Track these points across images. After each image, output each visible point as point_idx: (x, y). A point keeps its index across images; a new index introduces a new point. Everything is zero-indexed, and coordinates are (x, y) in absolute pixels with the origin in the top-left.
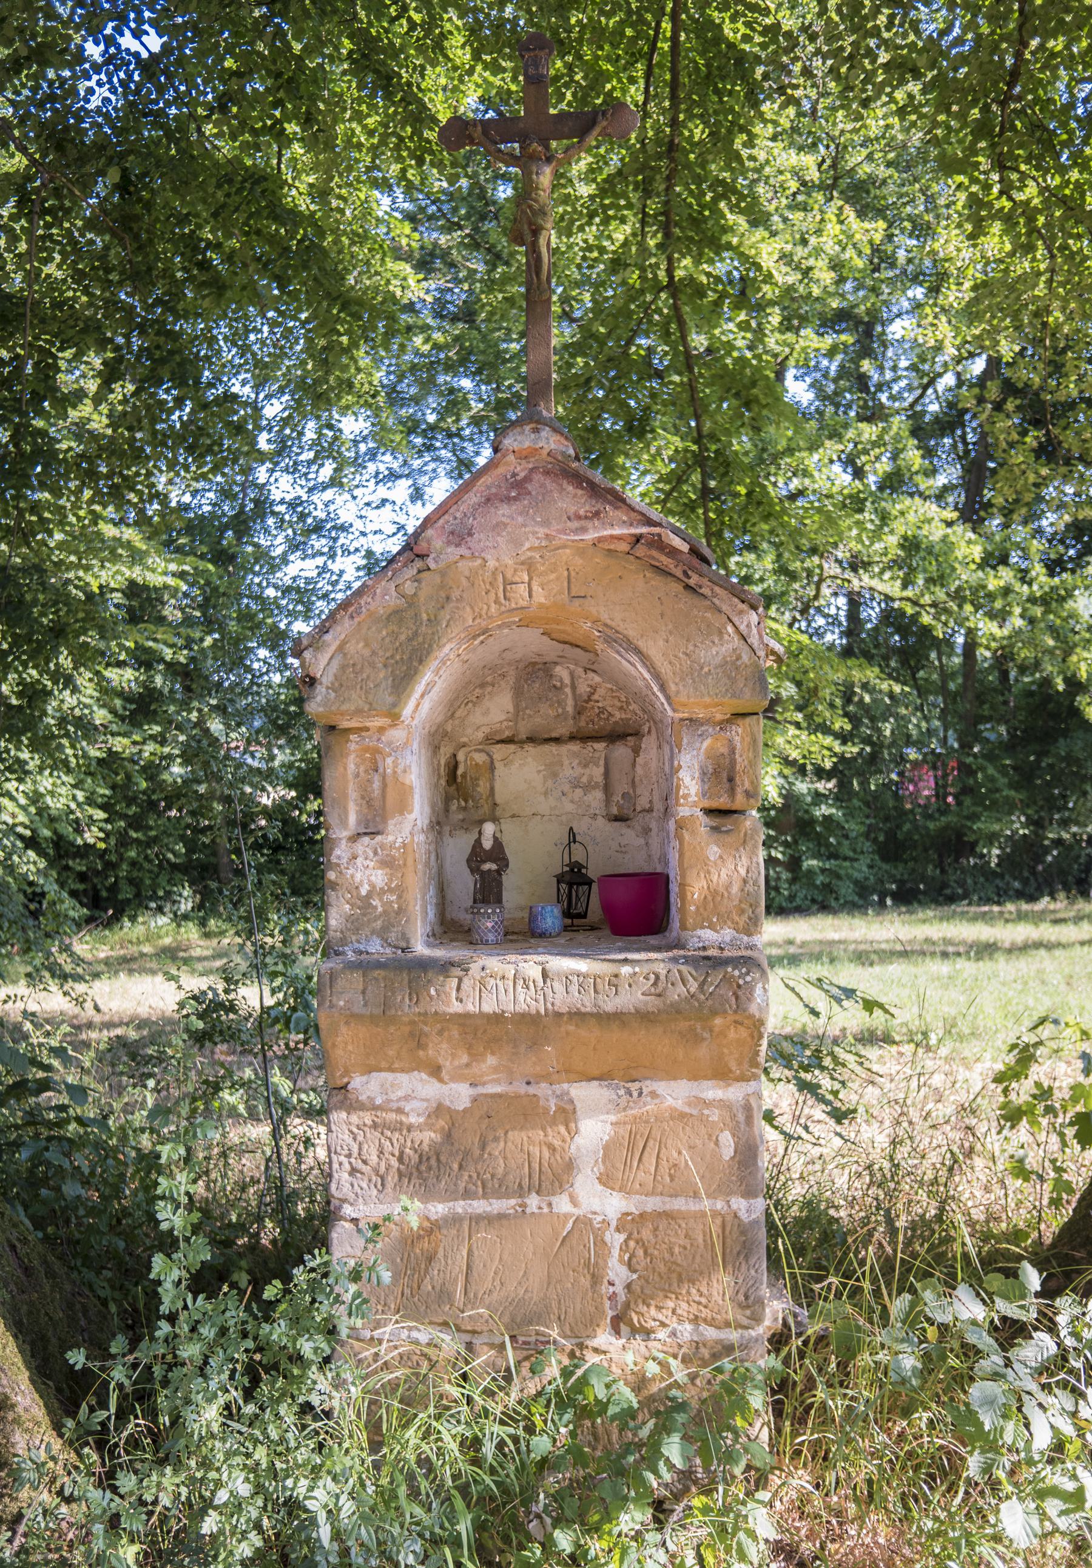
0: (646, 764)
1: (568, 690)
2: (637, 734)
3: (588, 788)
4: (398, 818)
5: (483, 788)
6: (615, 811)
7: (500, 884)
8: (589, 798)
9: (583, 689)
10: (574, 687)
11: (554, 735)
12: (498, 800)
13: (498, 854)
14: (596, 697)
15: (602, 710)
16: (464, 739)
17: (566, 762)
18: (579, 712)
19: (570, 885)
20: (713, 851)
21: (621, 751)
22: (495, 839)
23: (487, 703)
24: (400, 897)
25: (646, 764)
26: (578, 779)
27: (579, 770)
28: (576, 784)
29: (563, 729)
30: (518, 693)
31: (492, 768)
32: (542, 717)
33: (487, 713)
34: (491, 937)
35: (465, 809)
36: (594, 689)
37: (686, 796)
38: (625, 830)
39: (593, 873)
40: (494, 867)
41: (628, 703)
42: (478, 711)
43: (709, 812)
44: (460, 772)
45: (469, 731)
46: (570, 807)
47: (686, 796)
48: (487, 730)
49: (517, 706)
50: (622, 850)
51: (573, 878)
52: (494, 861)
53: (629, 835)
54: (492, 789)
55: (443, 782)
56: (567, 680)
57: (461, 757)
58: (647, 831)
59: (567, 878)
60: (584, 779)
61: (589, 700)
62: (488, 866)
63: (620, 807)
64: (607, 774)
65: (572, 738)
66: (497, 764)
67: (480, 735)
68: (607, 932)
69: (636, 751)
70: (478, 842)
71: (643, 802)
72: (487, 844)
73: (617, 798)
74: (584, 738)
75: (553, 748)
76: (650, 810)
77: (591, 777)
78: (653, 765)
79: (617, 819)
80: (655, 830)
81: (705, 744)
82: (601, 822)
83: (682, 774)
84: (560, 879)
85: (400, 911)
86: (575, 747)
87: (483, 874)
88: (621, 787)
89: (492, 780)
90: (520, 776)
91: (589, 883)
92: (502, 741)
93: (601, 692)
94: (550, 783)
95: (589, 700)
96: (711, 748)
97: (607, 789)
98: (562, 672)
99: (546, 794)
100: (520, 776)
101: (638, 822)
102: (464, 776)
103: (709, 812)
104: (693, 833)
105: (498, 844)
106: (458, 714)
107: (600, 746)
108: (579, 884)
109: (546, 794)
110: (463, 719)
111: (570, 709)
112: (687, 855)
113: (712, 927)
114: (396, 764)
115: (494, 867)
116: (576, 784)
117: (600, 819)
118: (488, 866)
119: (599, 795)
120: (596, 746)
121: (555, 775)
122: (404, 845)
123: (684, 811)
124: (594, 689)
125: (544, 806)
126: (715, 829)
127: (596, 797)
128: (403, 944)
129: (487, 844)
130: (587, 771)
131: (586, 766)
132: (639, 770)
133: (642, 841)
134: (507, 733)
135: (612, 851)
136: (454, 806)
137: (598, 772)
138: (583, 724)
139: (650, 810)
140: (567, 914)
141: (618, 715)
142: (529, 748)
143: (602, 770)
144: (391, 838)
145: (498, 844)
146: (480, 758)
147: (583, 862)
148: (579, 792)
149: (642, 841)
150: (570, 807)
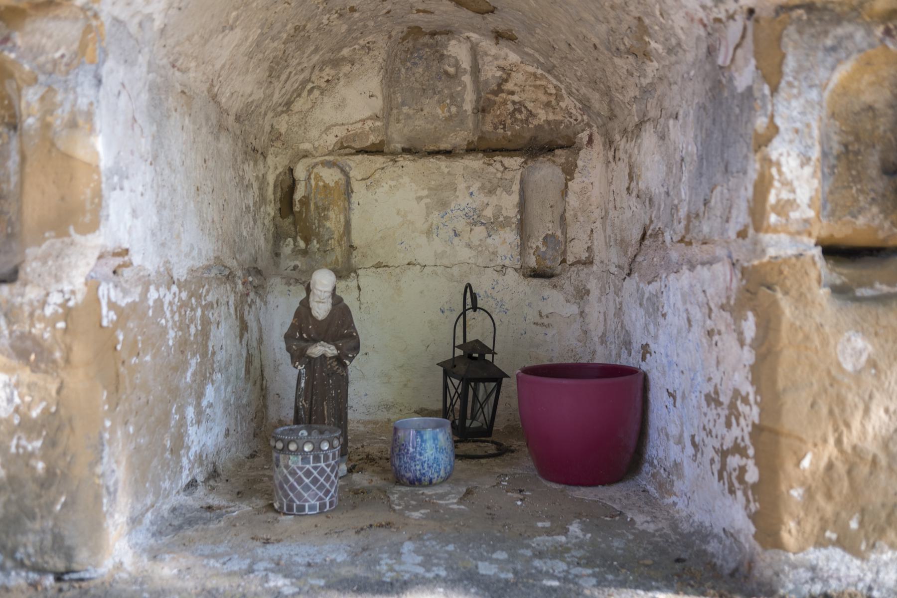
0: (584, 191)
1: (467, 79)
2: (570, 145)
3: (494, 225)
4: (51, 243)
5: (333, 222)
6: (532, 262)
7: (343, 383)
8: (495, 241)
9: (491, 72)
10: (476, 70)
11: (443, 146)
12: (356, 240)
13: (340, 327)
14: (509, 86)
15: (519, 107)
16: (306, 146)
17: (461, 186)
18: (482, 109)
19: (466, 381)
20: (853, 348)
21: (546, 172)
22: (337, 300)
23: (342, 90)
24: (51, 443)
25: (584, 191)
26: (478, 212)
27: (481, 198)
28: (475, 219)
29: (459, 138)
30: (391, 79)
31: (348, 192)
32: (426, 118)
33: (341, 105)
34: (311, 501)
35: (305, 253)
36: (507, 73)
37: (783, 208)
38: (548, 292)
39: (500, 361)
40: (331, 350)
41: (559, 97)
42: (328, 102)
43: (834, 252)
44: (299, 195)
45: (314, 133)
46: (465, 254)
47: (783, 208)
48: (341, 132)
49: (388, 98)
50: (543, 321)
51: (471, 367)
52: (331, 339)
53: (555, 300)
54: (348, 224)
55: (271, 210)
56: (466, 64)
57: (300, 172)
58: (582, 294)
59: (461, 368)
60: (489, 213)
61: (499, 90)
62: (318, 350)
63: (540, 257)
64: (522, 206)
65: (471, 150)
66: (356, 186)
67: (331, 140)
68: (525, 465)
69: (569, 171)
70: (305, 305)
71: (577, 250)
72: (321, 309)
73: (537, 243)
74: (486, 148)
75: (443, 164)
76: (589, 262)
77: (499, 208)
78: (596, 193)
79: (537, 274)
80: (595, 292)
81: (838, 76)
82: (512, 277)
83: (778, 149)
84: (449, 369)
85: (49, 480)
86: (475, 163)
87: (311, 363)
88: (543, 225)
89: (347, 210)
90: (391, 206)
91: (498, 377)
92: (360, 152)
93: (518, 78)
94: (435, 217)
95: (499, 90)
96: (843, 90)
97: (523, 228)
98: (458, 51)
99: (429, 233)
100: (391, 206)
101: (570, 279)
102: (305, 201)
103: (834, 252)
104: (801, 299)
105: (339, 307)
106: (298, 105)
107: (514, 162)
108: (478, 380)
109: (429, 233)
110: (304, 115)
111: (468, 107)
112: (788, 355)
113: (847, 543)
114: (48, 104)
115: (331, 350)
116: (475, 219)
117: (511, 272)
118: (318, 350)
119: (510, 236)
120: (507, 161)
121: (444, 204)
122: (68, 313)
123: (778, 246)
124: (507, 73)
125: (425, 251)
126: (840, 291)
127: (506, 241)
128: (60, 565)
129: (321, 309)
130: (493, 200)
131: (491, 192)
132: (573, 200)
133: (574, 309)
134: (372, 139)
135: (535, 324)
136: (287, 247)
137: (509, 203)
138: (488, 127)
139: (589, 262)
140: (462, 434)
141: (542, 116)
142: (406, 162)
143: (515, 198)
144: (32, 293)
145: (339, 307)
146: (330, 176)
147: (489, 344)
148: (480, 231)
149: (574, 309)
150: (465, 254)
